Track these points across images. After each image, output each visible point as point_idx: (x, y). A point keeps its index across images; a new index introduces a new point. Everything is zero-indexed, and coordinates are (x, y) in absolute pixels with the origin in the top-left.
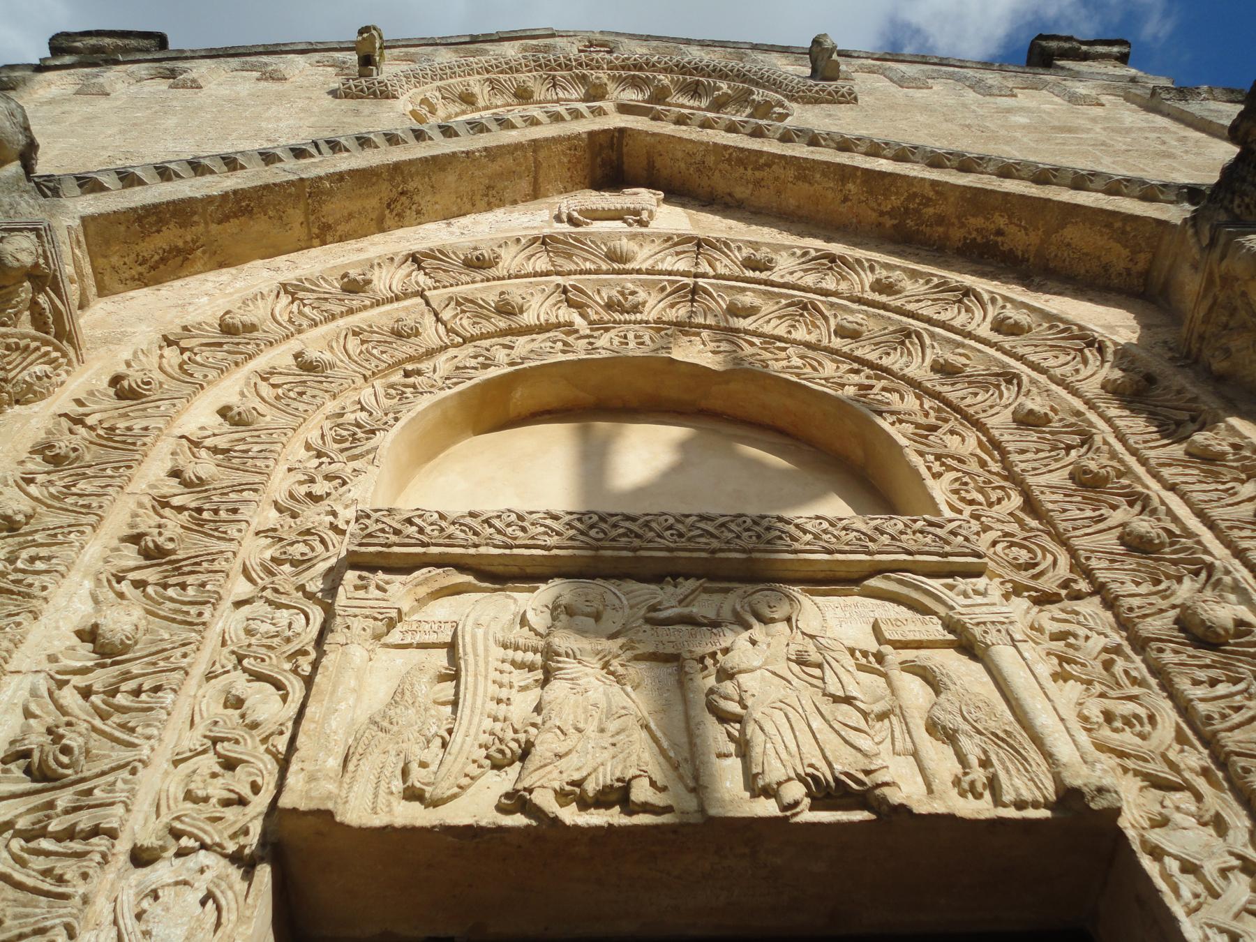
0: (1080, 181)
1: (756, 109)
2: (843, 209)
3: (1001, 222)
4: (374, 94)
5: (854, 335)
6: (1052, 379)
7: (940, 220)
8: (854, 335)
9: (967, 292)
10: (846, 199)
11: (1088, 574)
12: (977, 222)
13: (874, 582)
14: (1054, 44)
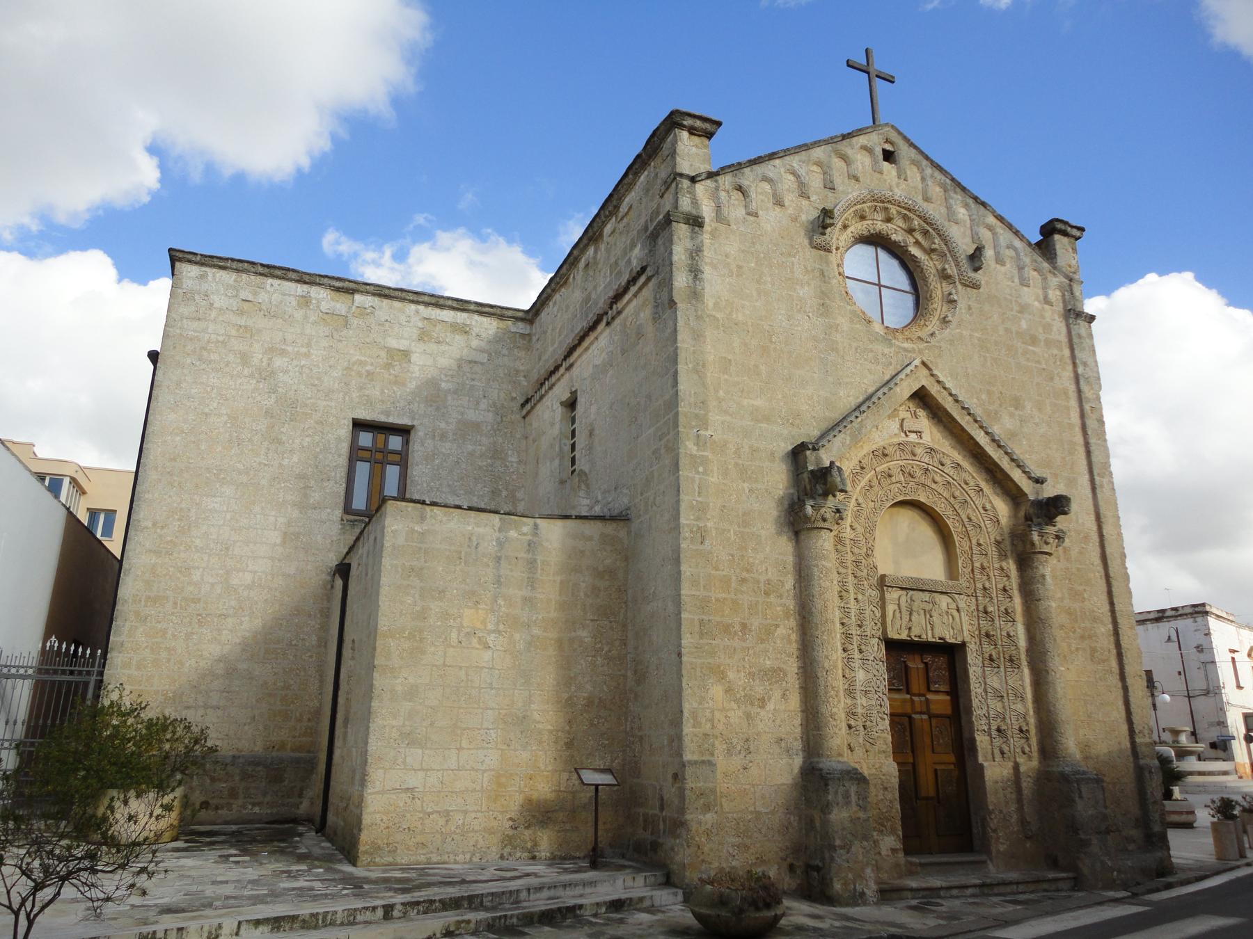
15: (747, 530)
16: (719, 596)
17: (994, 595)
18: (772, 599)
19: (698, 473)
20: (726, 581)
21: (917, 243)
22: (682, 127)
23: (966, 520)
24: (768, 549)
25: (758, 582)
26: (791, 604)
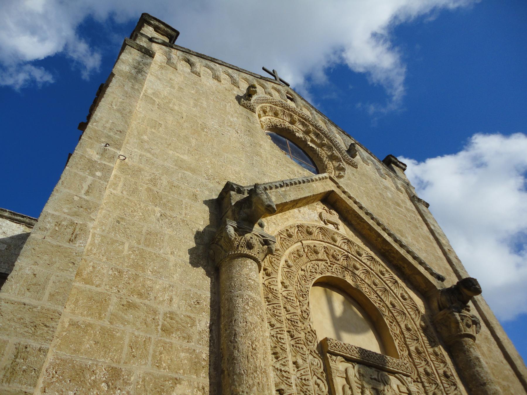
0: (421, 263)
1: (331, 155)
2: (375, 241)
3: (406, 266)
4: (250, 109)
5: (394, 306)
6: (411, 317)
7: (394, 257)
8: (376, 285)
9: (396, 282)
10: (376, 240)
11: (420, 378)
12: (401, 263)
13: (397, 375)
14: (393, 159)
15: (149, 249)
16: (80, 319)
17: (439, 381)
18: (175, 339)
19: (94, 175)
20: (99, 303)
21: (312, 141)
22: (150, 24)
23: (390, 306)
24: (176, 276)
25: (155, 312)
26: (204, 352)
